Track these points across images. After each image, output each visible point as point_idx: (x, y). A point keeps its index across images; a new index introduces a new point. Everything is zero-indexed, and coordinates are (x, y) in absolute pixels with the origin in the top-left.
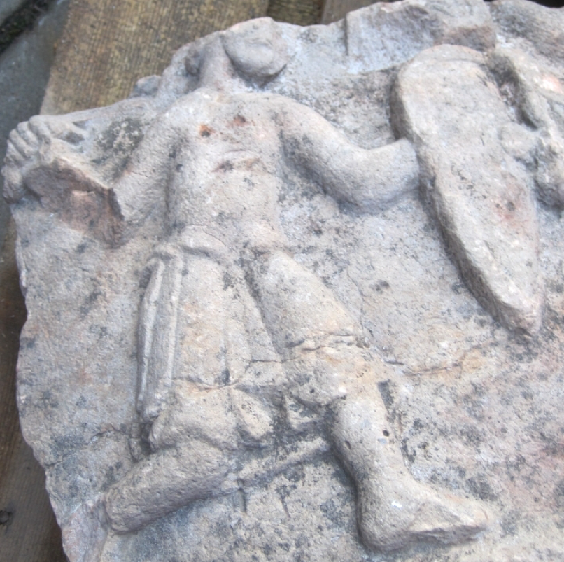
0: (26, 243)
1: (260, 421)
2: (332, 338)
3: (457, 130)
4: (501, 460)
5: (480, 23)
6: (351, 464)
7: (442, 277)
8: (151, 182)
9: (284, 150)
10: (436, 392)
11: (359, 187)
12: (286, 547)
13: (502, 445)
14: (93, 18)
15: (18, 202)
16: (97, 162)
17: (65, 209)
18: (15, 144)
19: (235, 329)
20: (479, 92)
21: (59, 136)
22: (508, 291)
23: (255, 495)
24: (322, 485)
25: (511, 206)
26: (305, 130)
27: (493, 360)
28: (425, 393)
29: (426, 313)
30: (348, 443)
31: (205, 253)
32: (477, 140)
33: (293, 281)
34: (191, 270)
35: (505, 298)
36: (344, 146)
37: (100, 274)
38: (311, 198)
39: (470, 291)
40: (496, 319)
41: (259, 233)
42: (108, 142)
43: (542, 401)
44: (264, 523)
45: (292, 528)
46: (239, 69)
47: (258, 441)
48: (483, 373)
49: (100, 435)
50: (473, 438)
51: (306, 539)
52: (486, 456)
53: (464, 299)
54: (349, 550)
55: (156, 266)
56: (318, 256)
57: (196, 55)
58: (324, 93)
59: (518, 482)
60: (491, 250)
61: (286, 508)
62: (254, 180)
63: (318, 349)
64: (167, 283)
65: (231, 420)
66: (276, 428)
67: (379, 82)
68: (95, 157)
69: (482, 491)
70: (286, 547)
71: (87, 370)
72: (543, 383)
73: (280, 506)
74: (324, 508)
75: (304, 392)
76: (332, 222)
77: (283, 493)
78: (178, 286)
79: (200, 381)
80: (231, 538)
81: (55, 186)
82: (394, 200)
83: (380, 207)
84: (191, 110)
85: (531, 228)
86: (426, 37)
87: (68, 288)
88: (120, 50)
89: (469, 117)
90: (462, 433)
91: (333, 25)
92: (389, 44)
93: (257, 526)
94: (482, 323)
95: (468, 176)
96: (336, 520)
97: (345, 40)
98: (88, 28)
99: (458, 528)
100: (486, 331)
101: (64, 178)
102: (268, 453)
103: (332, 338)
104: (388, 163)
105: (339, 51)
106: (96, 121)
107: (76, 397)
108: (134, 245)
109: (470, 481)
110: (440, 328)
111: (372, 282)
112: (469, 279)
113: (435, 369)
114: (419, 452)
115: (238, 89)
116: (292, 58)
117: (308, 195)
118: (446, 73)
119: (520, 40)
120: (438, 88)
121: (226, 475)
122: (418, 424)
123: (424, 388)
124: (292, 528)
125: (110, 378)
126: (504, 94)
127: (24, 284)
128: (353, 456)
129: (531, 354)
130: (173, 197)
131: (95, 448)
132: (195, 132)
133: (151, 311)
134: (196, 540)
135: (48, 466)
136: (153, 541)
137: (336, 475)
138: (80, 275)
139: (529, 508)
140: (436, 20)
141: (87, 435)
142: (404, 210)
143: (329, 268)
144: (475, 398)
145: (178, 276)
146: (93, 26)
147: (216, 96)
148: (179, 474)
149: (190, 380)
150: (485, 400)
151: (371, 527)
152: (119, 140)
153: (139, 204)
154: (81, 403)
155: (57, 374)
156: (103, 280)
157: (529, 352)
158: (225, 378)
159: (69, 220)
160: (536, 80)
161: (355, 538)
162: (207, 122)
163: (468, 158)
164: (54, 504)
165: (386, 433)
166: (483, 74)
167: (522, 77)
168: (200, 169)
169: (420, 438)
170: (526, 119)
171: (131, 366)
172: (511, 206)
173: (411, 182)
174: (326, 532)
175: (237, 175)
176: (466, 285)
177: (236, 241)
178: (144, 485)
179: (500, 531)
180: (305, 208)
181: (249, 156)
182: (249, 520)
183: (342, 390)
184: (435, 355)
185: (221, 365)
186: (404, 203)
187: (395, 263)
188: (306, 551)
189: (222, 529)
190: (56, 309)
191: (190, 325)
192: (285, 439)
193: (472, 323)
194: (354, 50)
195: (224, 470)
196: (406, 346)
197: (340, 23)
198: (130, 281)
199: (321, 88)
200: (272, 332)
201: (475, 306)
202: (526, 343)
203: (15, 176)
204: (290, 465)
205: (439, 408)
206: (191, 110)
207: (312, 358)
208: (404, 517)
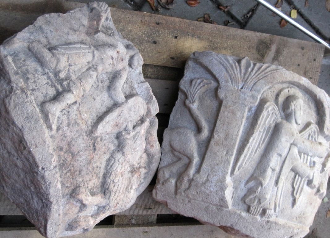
0: (80, 10)
1: (62, 75)
2: (84, 88)
3: (130, 111)
4: (65, 132)
5: (152, 113)
6: (59, 98)
7: (99, 112)
8: (104, 41)
9: (117, 71)
10: (76, 115)
11: (114, 90)
12: (36, 86)
13: (68, 132)
14: (130, 17)
15: (88, 6)
16: (103, 26)
17: (91, 19)
18: (102, 4)
19: (80, 66)
20: (138, 115)
21: (107, 15)
22: (100, 127)
23: (45, 77)
24: (52, 92)
25: (117, 125)
26: (123, 75)
27: (85, 127)
28: (75, 112)
29: (91, 110)
30: (64, 96)
31: (94, 56)
32: (129, 116)
33: (93, 78)
34: (90, 54)
35: (99, 127)
36: (121, 84)
37: (80, 31)
38: (108, 79)
39: (97, 119)
40: (93, 126)
41: (100, 68)
42: (108, 28)
43: (79, 140)
44: (40, 80)
45: (41, 87)
46: (132, 58)
47: (58, 76)
48: (82, 125)
49: (46, 37)
50: (68, 125)
51: (39, 90)
52: (65, 128)
53: (96, 118)
54: (39, 101)
55: (87, 45)
56: (97, 83)
57: (132, 47)
58: (130, 79)
59: (61, 137)
60: (108, 122)
61: (44, 85)
62: (111, 65)
63: (81, 86)
64: (85, 49)
65: (62, 68)
66: (61, 79)
67: (134, 92)
68: (104, 25)
69: (58, 129)
70: (36, 86)
71: (59, 32)
72: (82, 139)
73: (45, 83)
74: (47, 93)
75: (71, 84)
76: (104, 85)
77: (48, 83)
78: (86, 51)
79: (69, 60)
80: (35, 73)
81: (95, 16)
82: (112, 99)
83: (110, 96)
84: (122, 48)
85: (113, 131)
86: (147, 101)
87: (74, 24)
88: (123, 26)
89: (133, 113)
90: (69, 122)
91: (144, 79)
92: (143, 93)
93: (39, 79)
94: (91, 123)
95: (121, 115)
96: (45, 96)
97: (141, 82)
98: (128, 16)
99: (51, 124)
100: (90, 124)
101: (98, 18)
102: (55, 78)
103: (84, 88)
104: (121, 97)
105: (139, 81)
106: (111, 24)
107: (52, 30)
108: (88, 39)
109: (60, 126)
110: (89, 114)
111: (95, 96)
112: (100, 118)
113: (80, 114)
114: (63, 113)
115: (128, 58)
116: (135, 70)
117: (109, 79)
118: (141, 107)
119: (149, 124)
120: (137, 105)
121: (49, 69)
122: (69, 112)
123: (76, 112)
124: (41, 87)
125: (59, 38)
126: (138, 121)
127: (71, 12)
128: (61, 97)
129: (87, 136)
130: (102, 47)
131: (43, 37)
132: (118, 50)
133: (78, 46)
134: (32, 65)
135: (34, 25)
136: (28, 54)
137: (54, 95)
138: (78, 26)
139: (56, 141)
140: (151, 103)
141: (45, 34)
142: (110, 102)
143: (95, 86)
144: (77, 124)
145: (87, 51)
146: (128, 17)
147: (125, 53)
148: (48, 58)
149: (68, 58)
150: (77, 126)
151: (47, 105)
152: (109, 31)
153: (98, 39)
154: (51, 32)
155: (55, 24)
156: (79, 32)
157: (88, 135)
158: (70, 66)
159: (89, 21)
160: (143, 128)
161: (42, 102)
162: (120, 52)
163: (125, 114)
164: (27, 28)
165: (68, 104)
166: (142, 116)
167: (143, 124)
168: (111, 52)
169: (66, 113)
170: (134, 127)
171: (63, 43)
172: (117, 125)
173: (117, 102)
174: (42, 95)
175: (111, 61)
176: (98, 118)
177: (97, 63)
178: (43, 50)
179: (51, 135)
180: (106, 79)
181: (115, 63)
182: (40, 77)
183: (74, 93)
184: (83, 113)
185: (73, 64)
186: (112, 101)
187: (99, 101)
188: (37, 91)
189: (36, 70)
190: (69, 21)
191: (79, 56)
192: (60, 82)
193: (91, 121)
194: (140, 85)
195: (50, 69)
196: (84, 106)
197: (145, 81)
198: (81, 39)
199: (130, 78)
200: (81, 74)
201: (95, 121)
202: (90, 134)
203: (95, 5)
204: (54, 84)
205: (73, 116)
206: (122, 48)
207: (79, 85)
208: (52, 111)
